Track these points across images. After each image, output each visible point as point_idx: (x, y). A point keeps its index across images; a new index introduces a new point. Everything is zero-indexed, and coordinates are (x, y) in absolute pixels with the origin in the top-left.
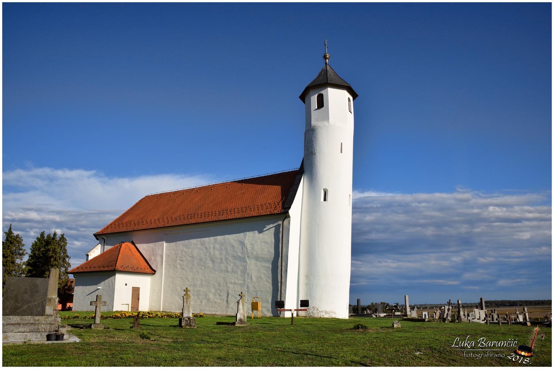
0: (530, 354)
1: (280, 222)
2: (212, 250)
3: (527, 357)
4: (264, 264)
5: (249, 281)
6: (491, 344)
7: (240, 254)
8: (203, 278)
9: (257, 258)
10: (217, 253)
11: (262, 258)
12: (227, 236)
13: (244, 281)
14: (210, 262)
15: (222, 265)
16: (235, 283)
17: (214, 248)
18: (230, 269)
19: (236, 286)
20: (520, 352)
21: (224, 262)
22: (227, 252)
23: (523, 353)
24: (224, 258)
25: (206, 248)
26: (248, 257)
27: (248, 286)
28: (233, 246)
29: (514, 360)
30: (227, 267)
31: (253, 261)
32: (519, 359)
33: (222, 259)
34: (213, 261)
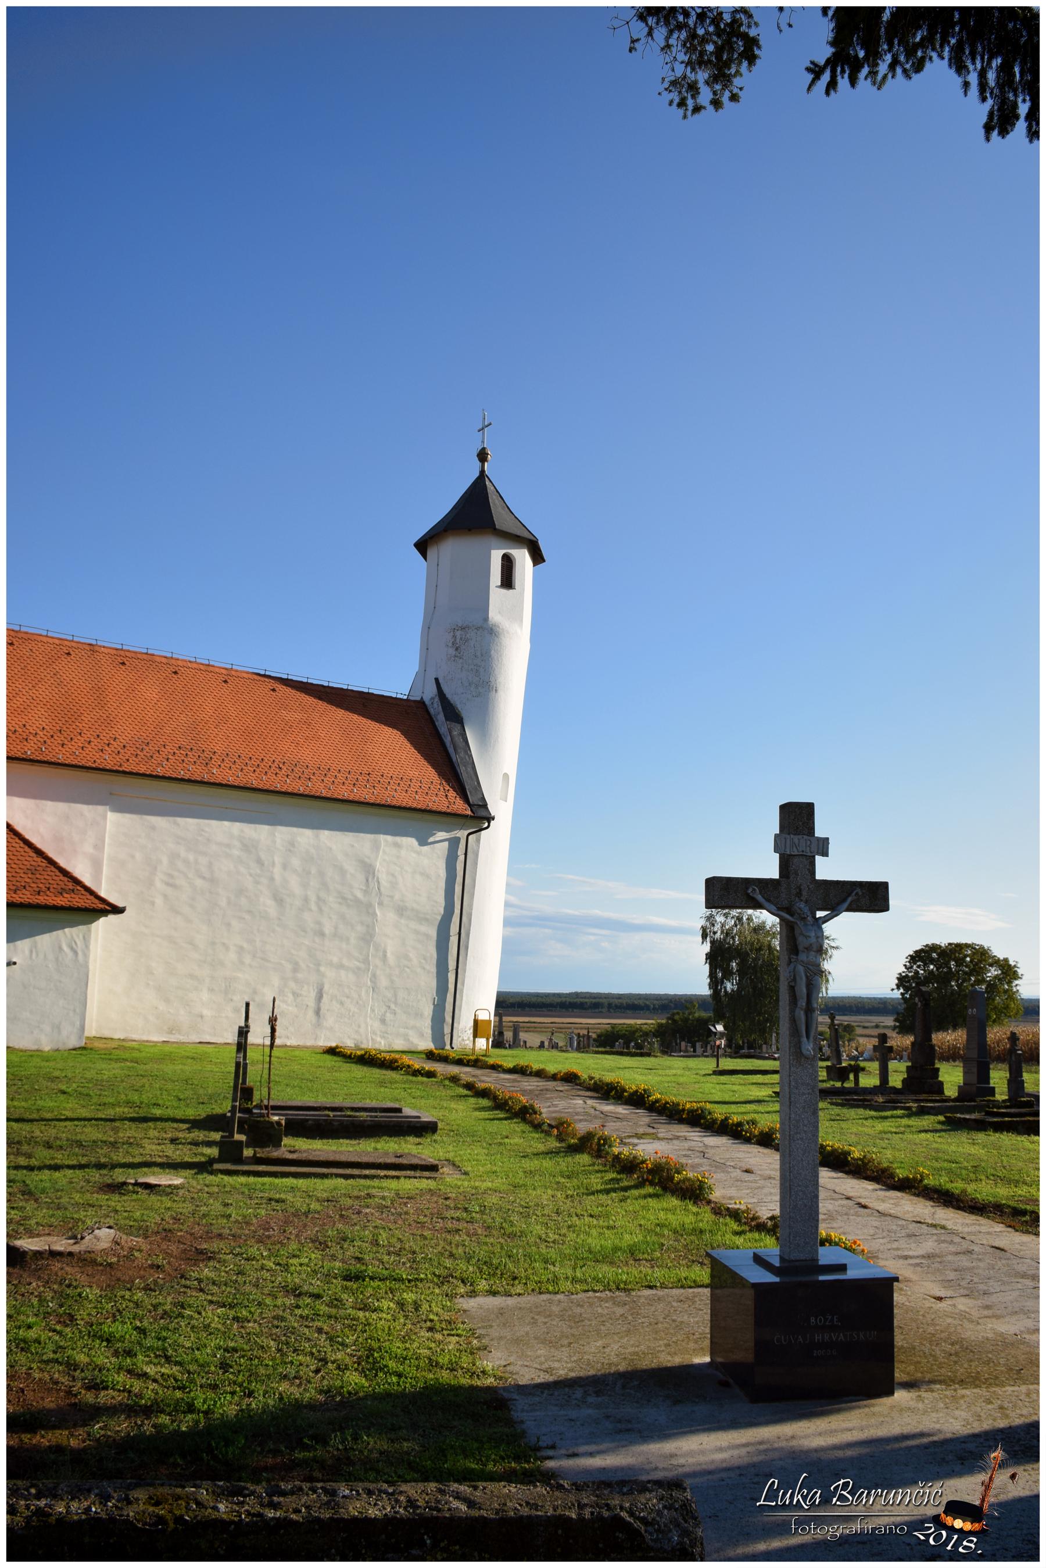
0: (977, 1526)
1: (462, 834)
3: (971, 1533)
9: (401, 911)
17: (285, 867)
18: (328, 929)
20: (949, 1520)
23: (958, 1524)
28: (343, 872)
29: (932, 1542)
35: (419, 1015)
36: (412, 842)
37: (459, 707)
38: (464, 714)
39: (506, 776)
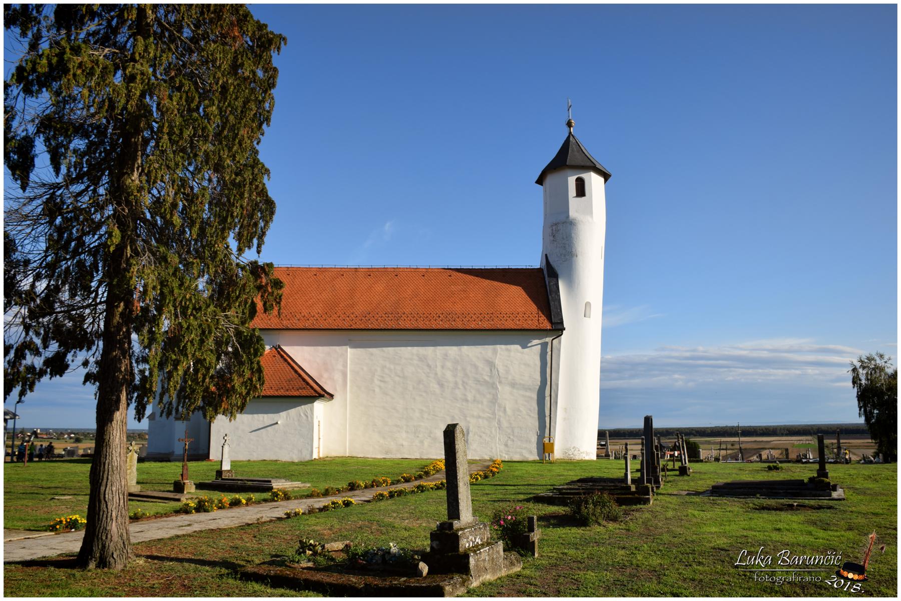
0: (861, 577)
1: (549, 340)
2: (439, 369)
3: (858, 581)
4: (528, 394)
5: (501, 414)
6: (799, 560)
7: (487, 378)
8: (424, 409)
9: (513, 385)
10: (449, 375)
11: (520, 384)
12: (465, 349)
13: (494, 413)
14: (436, 386)
15: (457, 392)
16: (479, 417)
17: (443, 367)
18: (470, 397)
19: (480, 420)
20: (845, 574)
21: (460, 386)
22: (466, 375)
23: (851, 576)
24: (460, 383)
25: (429, 366)
26: (500, 382)
27: (499, 421)
28: (476, 367)
29: (835, 586)
30: (465, 395)
31: (508, 389)
32: (845, 585)
33: (456, 383)
34: (441, 385)
35: (528, 441)
36: (518, 347)
37: (556, 268)
38: (559, 272)
39: (588, 305)
